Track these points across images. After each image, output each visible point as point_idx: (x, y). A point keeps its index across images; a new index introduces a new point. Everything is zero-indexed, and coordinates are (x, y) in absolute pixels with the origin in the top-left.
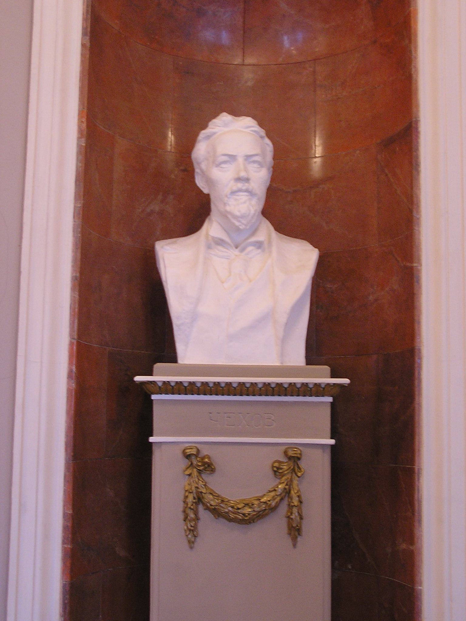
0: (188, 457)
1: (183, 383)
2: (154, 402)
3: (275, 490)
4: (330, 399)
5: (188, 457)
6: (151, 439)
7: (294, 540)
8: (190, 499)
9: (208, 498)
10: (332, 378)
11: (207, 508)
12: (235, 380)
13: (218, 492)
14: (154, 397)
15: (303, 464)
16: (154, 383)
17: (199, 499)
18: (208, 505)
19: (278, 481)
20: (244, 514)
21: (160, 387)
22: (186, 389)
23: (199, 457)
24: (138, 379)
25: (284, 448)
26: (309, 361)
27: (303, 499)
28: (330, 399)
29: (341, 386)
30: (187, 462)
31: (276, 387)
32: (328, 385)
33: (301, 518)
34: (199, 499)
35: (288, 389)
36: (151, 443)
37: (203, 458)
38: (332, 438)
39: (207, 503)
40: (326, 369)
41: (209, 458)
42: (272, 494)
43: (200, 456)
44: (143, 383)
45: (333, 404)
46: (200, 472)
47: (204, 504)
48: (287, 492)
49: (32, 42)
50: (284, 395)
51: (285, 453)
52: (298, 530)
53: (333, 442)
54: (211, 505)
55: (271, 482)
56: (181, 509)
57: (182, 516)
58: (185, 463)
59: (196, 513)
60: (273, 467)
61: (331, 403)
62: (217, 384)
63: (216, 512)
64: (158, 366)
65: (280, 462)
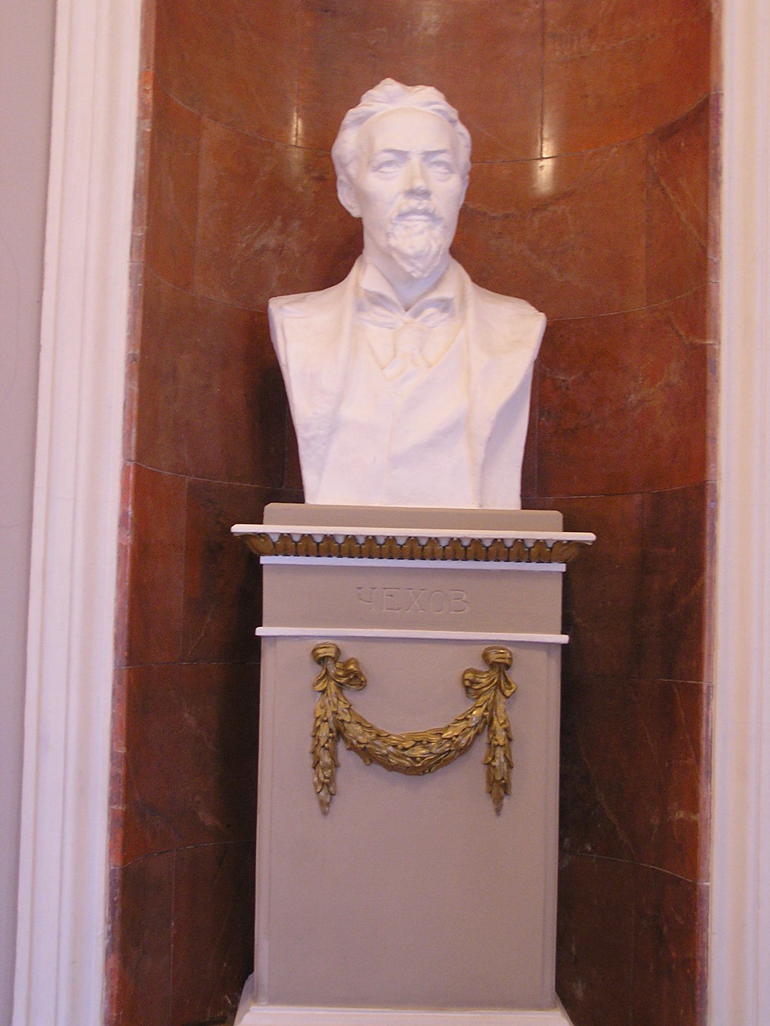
0: (321, 661)
2: (264, 568)
3: (466, 719)
4: (562, 567)
5: (321, 661)
6: (259, 631)
7: (498, 803)
8: (324, 732)
9: (354, 730)
11: (352, 748)
12: (341, 531)
13: (370, 719)
14: (264, 560)
15: (514, 675)
17: (339, 733)
18: (355, 742)
19: (473, 703)
20: (414, 759)
21: (274, 544)
24: (237, 528)
25: (483, 648)
26: (526, 504)
27: (513, 734)
28: (562, 567)
29: (580, 545)
30: (319, 670)
32: (559, 542)
33: (510, 766)
34: (339, 733)
36: (259, 637)
37: (346, 664)
38: (563, 633)
40: (556, 516)
41: (357, 663)
42: (462, 725)
44: (246, 536)
46: (340, 686)
47: (346, 740)
48: (487, 722)
51: (485, 656)
52: (505, 787)
53: (565, 639)
54: (359, 743)
55: (459, 705)
56: (309, 748)
57: (310, 761)
58: (313, 672)
59: (334, 756)
60: (464, 680)
61: (563, 573)
62: (351, 539)
63: (367, 754)
64: (271, 508)
65: (475, 672)
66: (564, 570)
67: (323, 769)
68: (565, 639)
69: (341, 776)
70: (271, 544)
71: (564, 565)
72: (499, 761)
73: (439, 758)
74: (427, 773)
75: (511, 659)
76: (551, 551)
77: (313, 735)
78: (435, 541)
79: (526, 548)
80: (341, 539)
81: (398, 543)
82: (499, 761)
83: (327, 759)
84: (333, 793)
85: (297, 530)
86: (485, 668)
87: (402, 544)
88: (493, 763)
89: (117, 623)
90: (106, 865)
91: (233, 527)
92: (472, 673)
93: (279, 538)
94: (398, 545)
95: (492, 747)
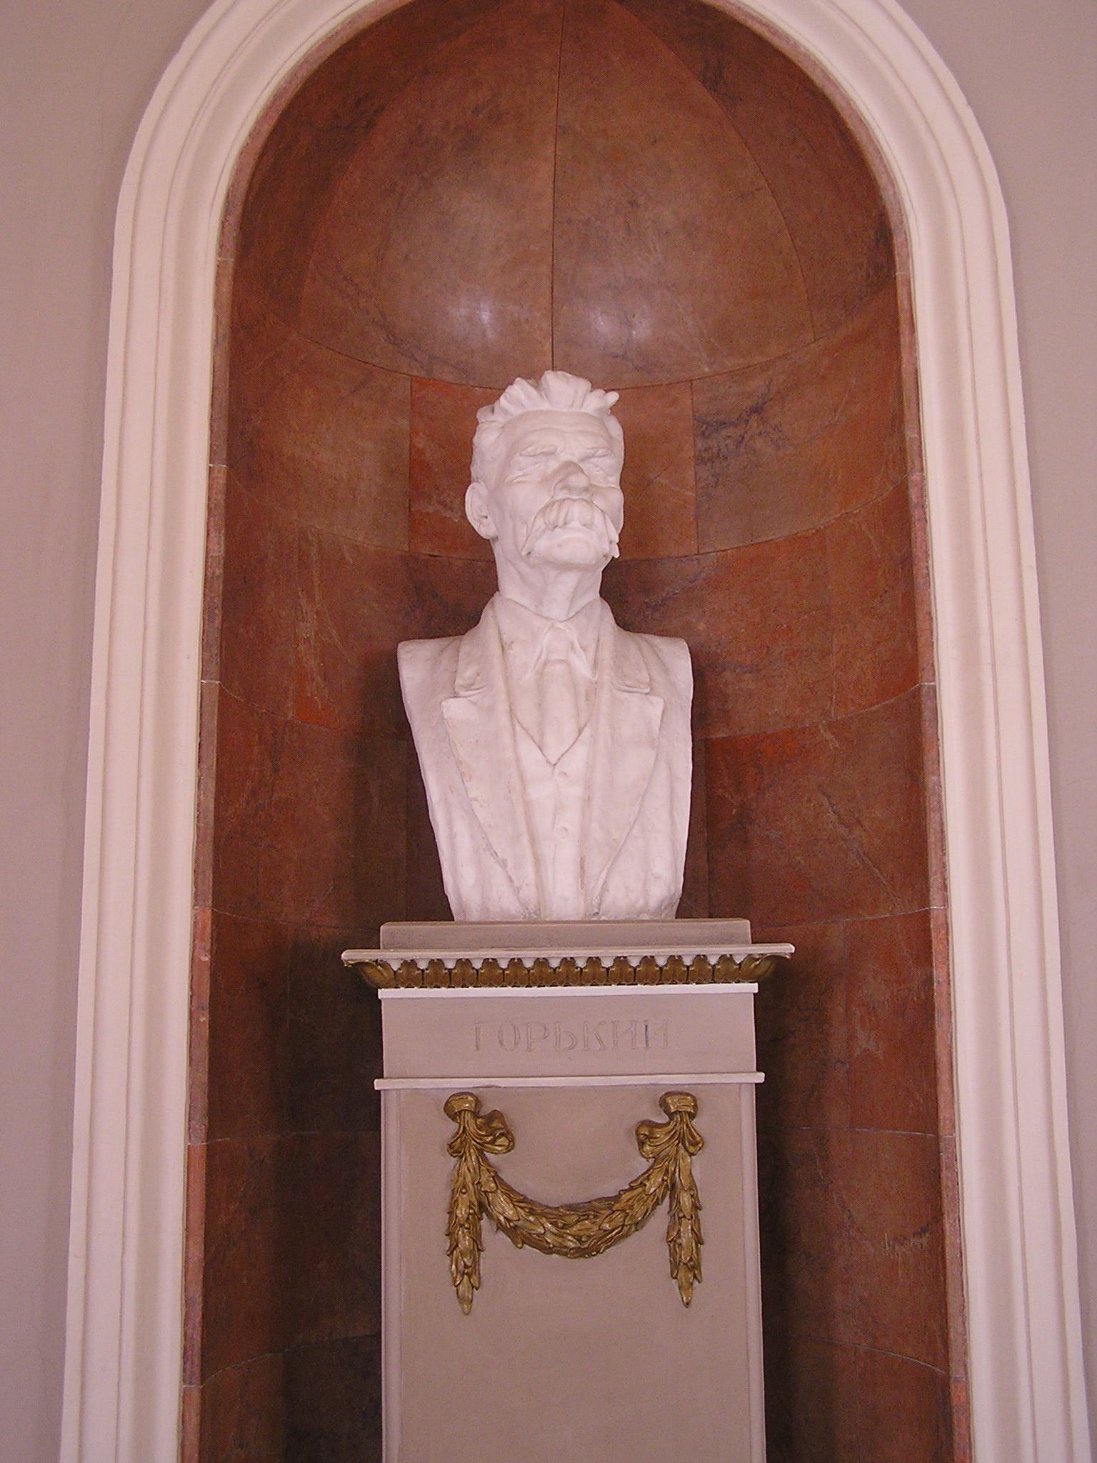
1: (445, 962)
4: (754, 987)
8: (462, 1212)
10: (753, 943)
11: (500, 1227)
14: (383, 993)
16: (385, 965)
18: (501, 1218)
22: (450, 974)
23: (481, 1117)
26: (676, 918)
27: (703, 1199)
28: (754, 987)
31: (455, 967)
32: (751, 958)
33: (699, 1241)
35: (480, 971)
38: (758, 1070)
39: (498, 1214)
40: (743, 926)
43: (483, 1114)
44: (361, 965)
45: (759, 1000)
47: (490, 1216)
49: (192, 940)
50: (710, 980)
52: (694, 1268)
56: (443, 1228)
59: (477, 1240)
61: (755, 994)
63: (514, 1232)
66: (757, 991)
67: (462, 1254)
68: (760, 1077)
69: (486, 1264)
70: (392, 973)
71: (756, 985)
72: (686, 1237)
73: (610, 1236)
74: (594, 1255)
75: (695, 1107)
76: (740, 968)
77: (450, 1211)
78: (467, 962)
79: (684, 966)
80: (452, 964)
81: (603, 966)
82: (686, 1237)
83: (465, 1242)
84: (477, 1285)
85: (423, 958)
86: (663, 1119)
87: (635, 966)
88: (679, 1241)
89: (238, 171)
90: (178, 1425)
91: (343, 955)
92: (648, 1126)
93: (640, 963)
94: (603, 968)
95: (676, 1216)
